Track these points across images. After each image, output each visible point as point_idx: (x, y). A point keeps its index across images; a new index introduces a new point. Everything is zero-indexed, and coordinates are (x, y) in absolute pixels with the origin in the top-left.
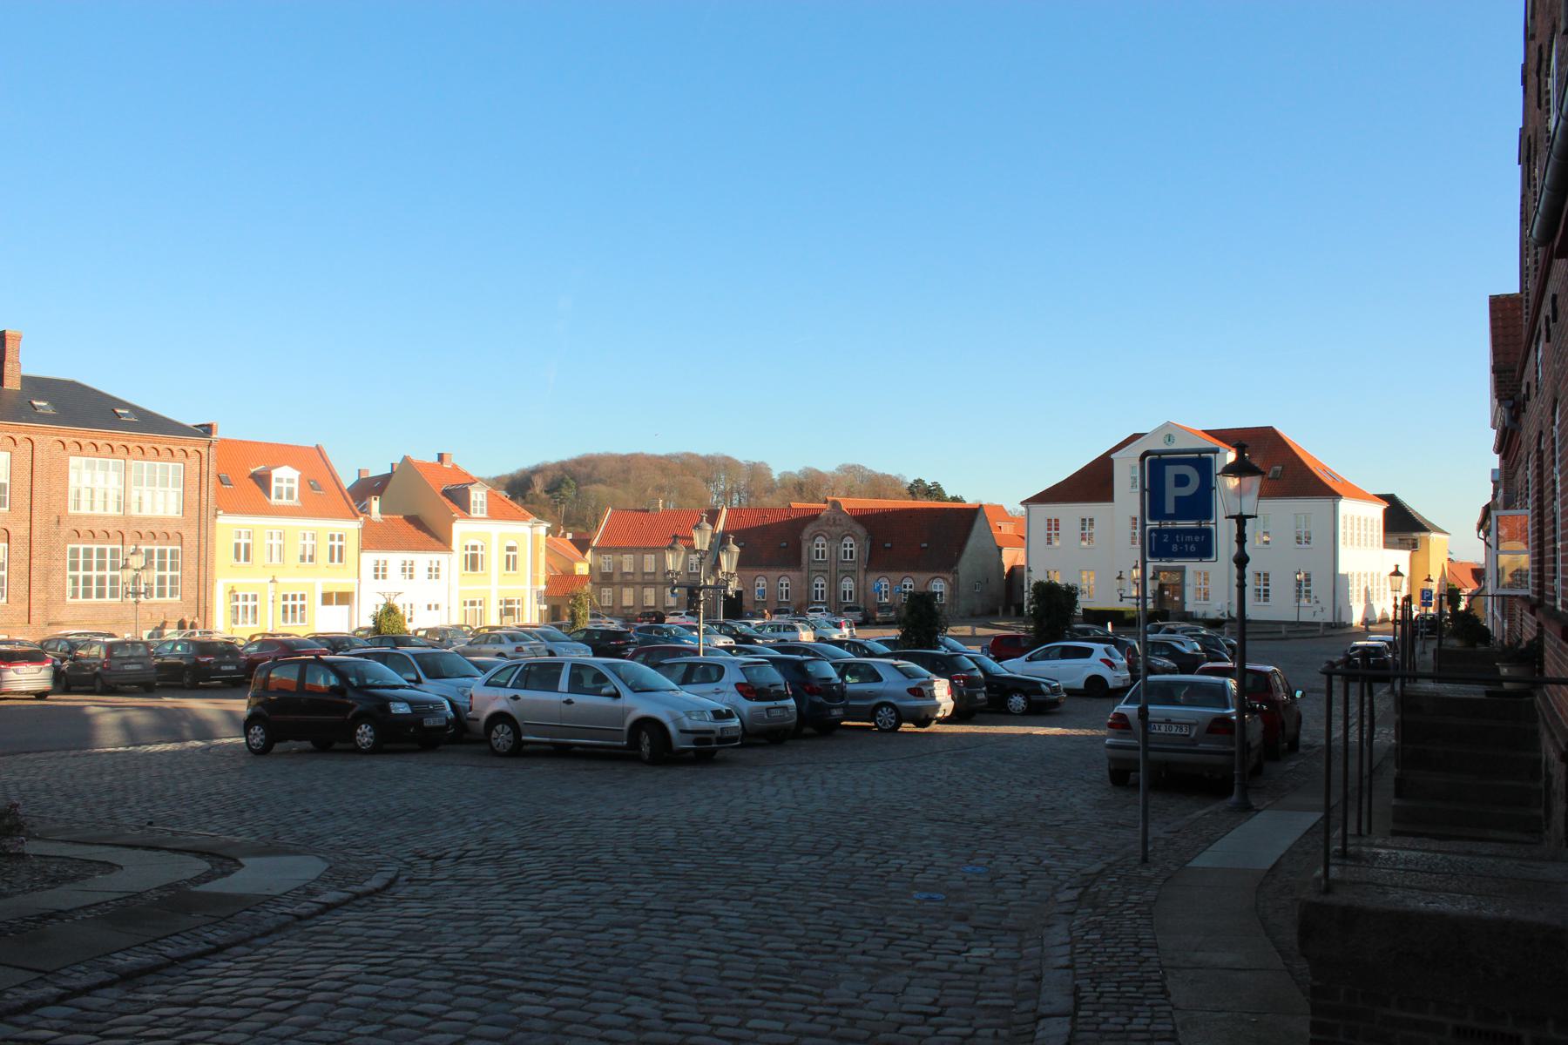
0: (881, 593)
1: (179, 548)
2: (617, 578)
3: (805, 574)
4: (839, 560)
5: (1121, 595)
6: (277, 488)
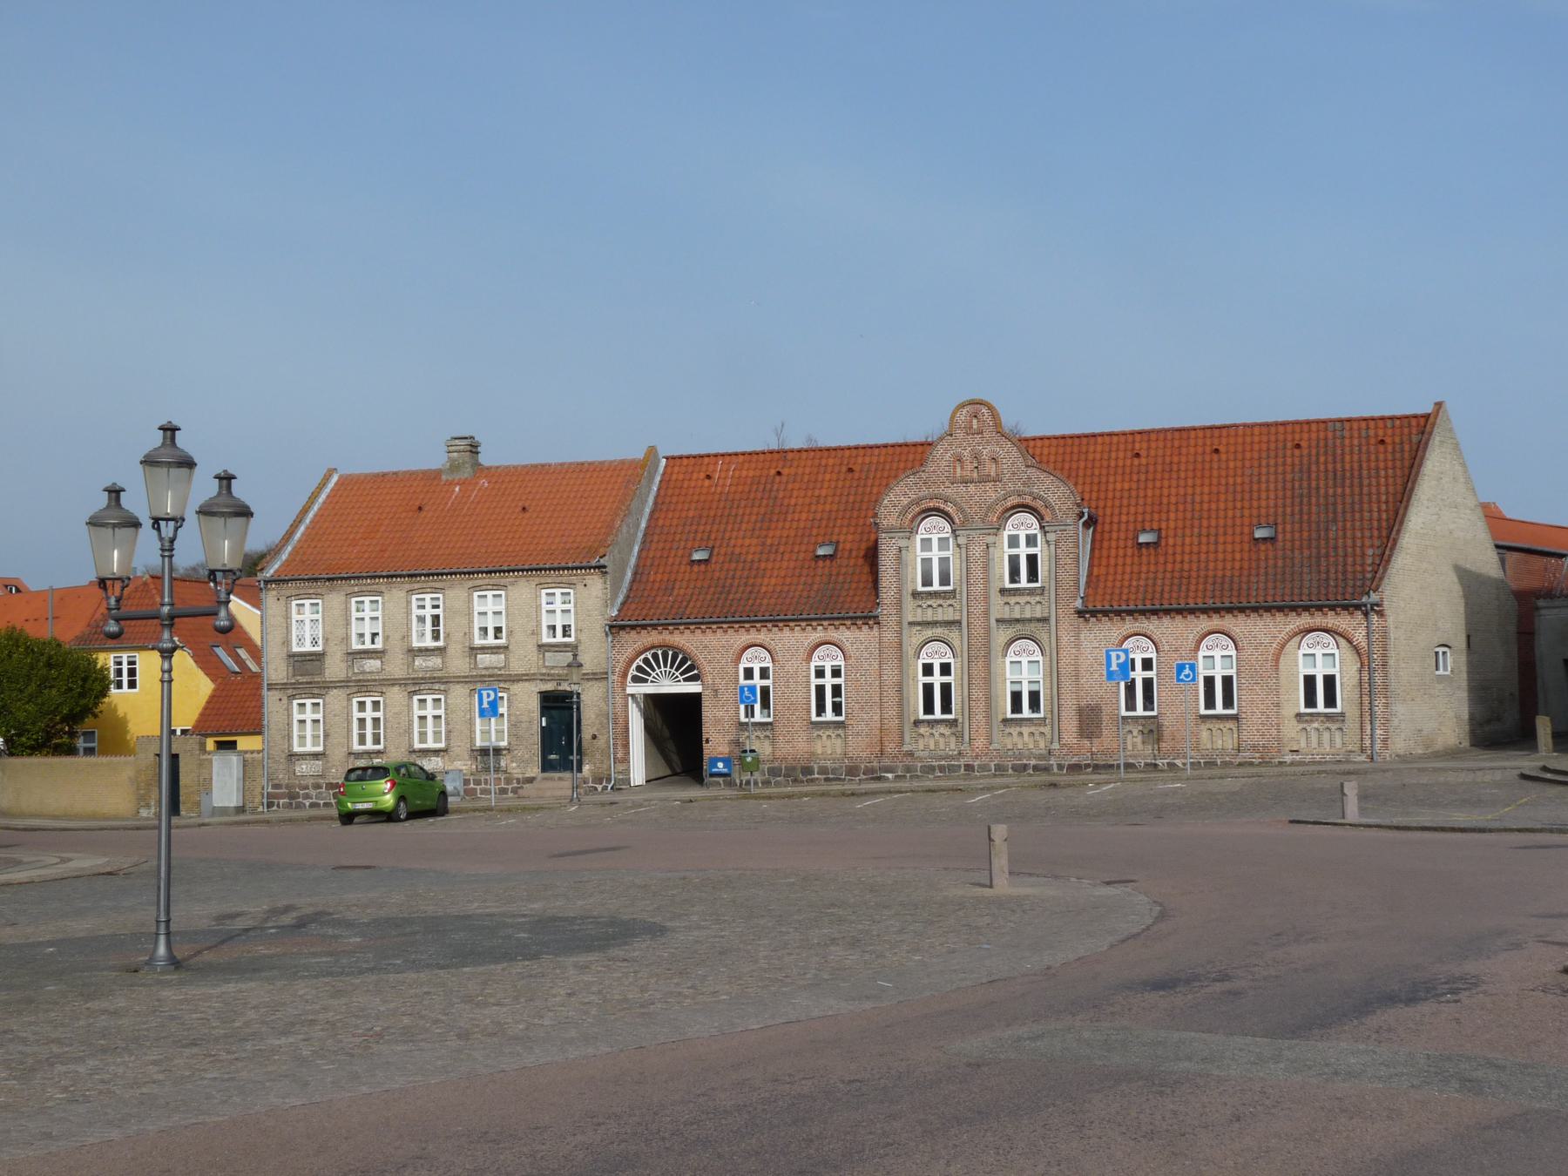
0: (1130, 688)
2: (335, 668)
3: (889, 636)
4: (995, 587)
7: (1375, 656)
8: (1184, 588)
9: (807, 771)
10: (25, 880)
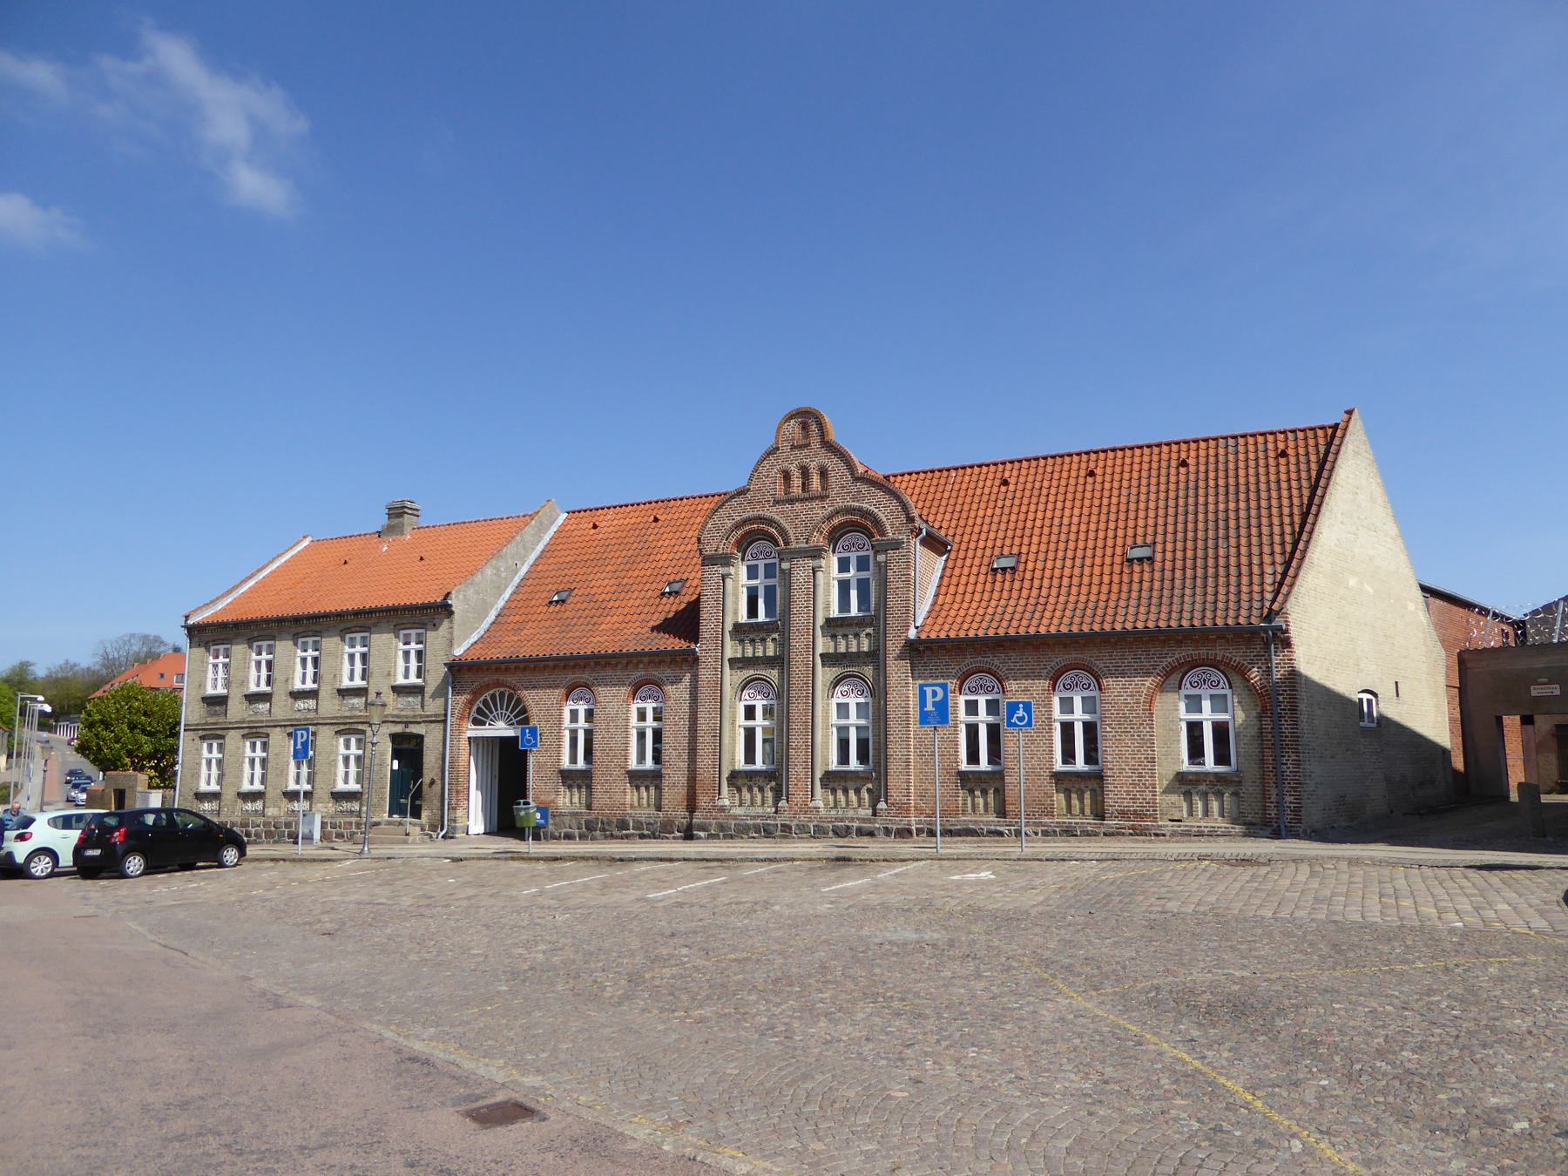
7: (1281, 698)
8: (1037, 615)
9: (623, 825)
10: (693, 857)
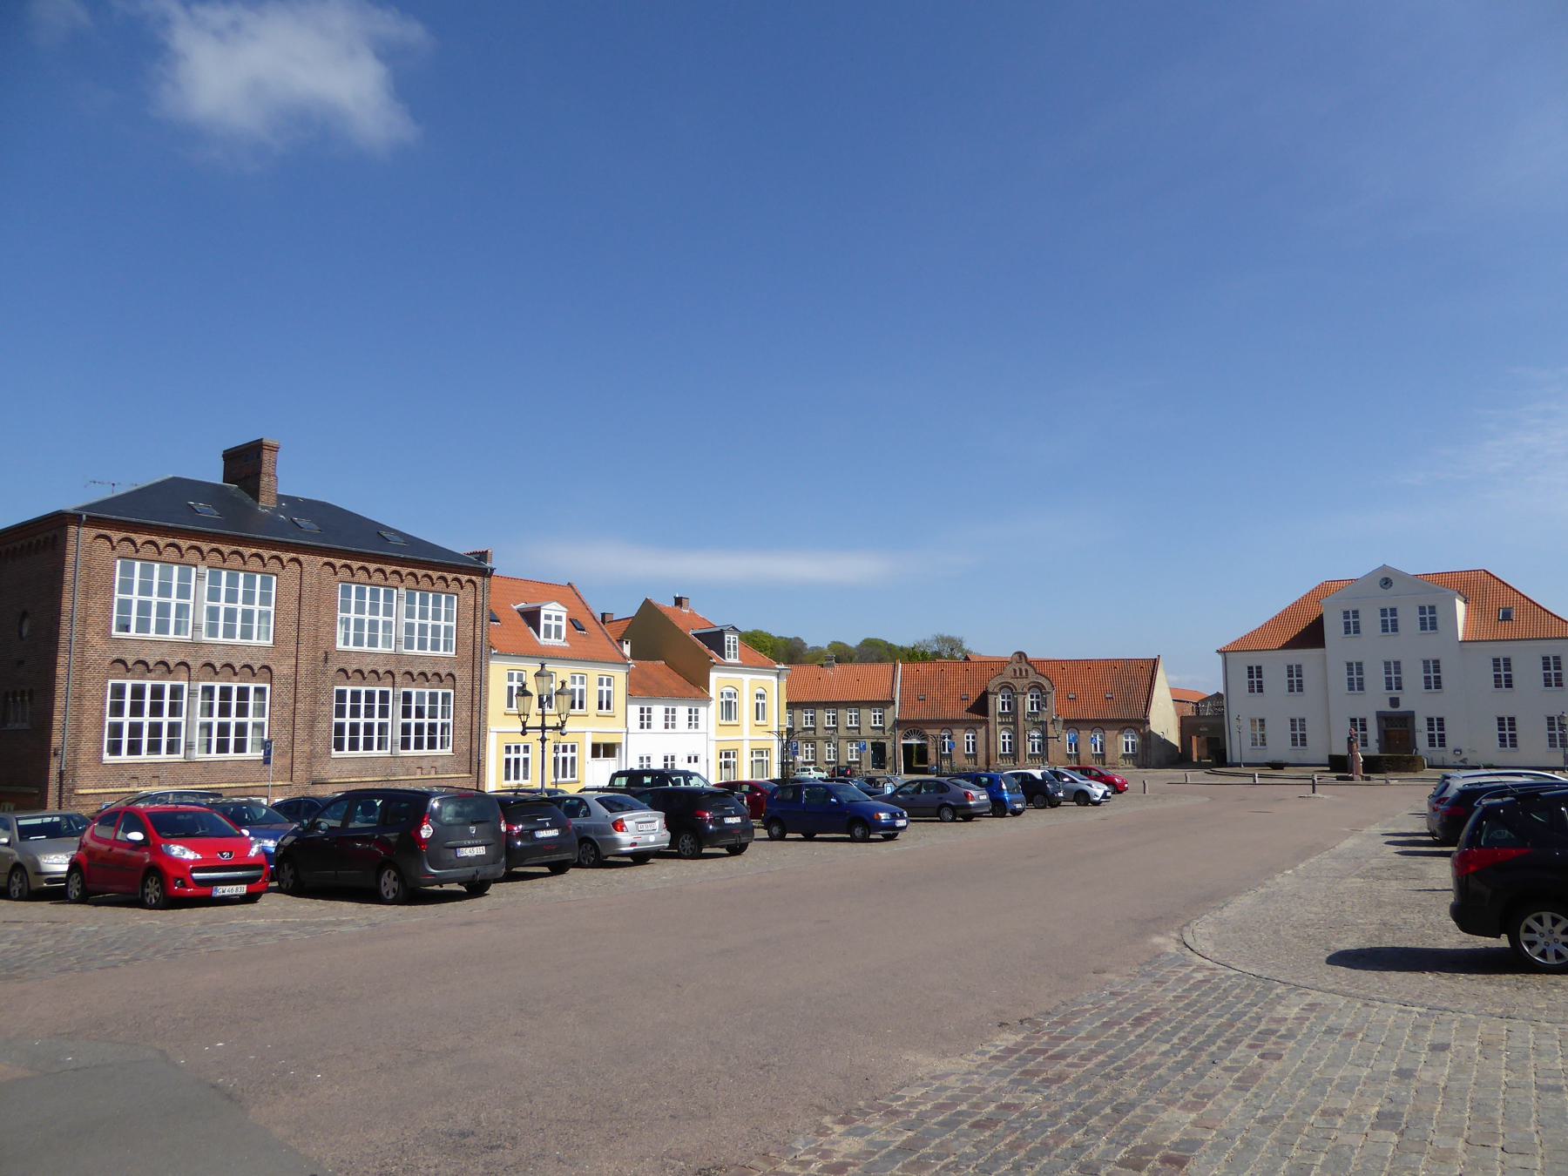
1: (452, 692)
5: (524, 724)
6: (545, 625)
